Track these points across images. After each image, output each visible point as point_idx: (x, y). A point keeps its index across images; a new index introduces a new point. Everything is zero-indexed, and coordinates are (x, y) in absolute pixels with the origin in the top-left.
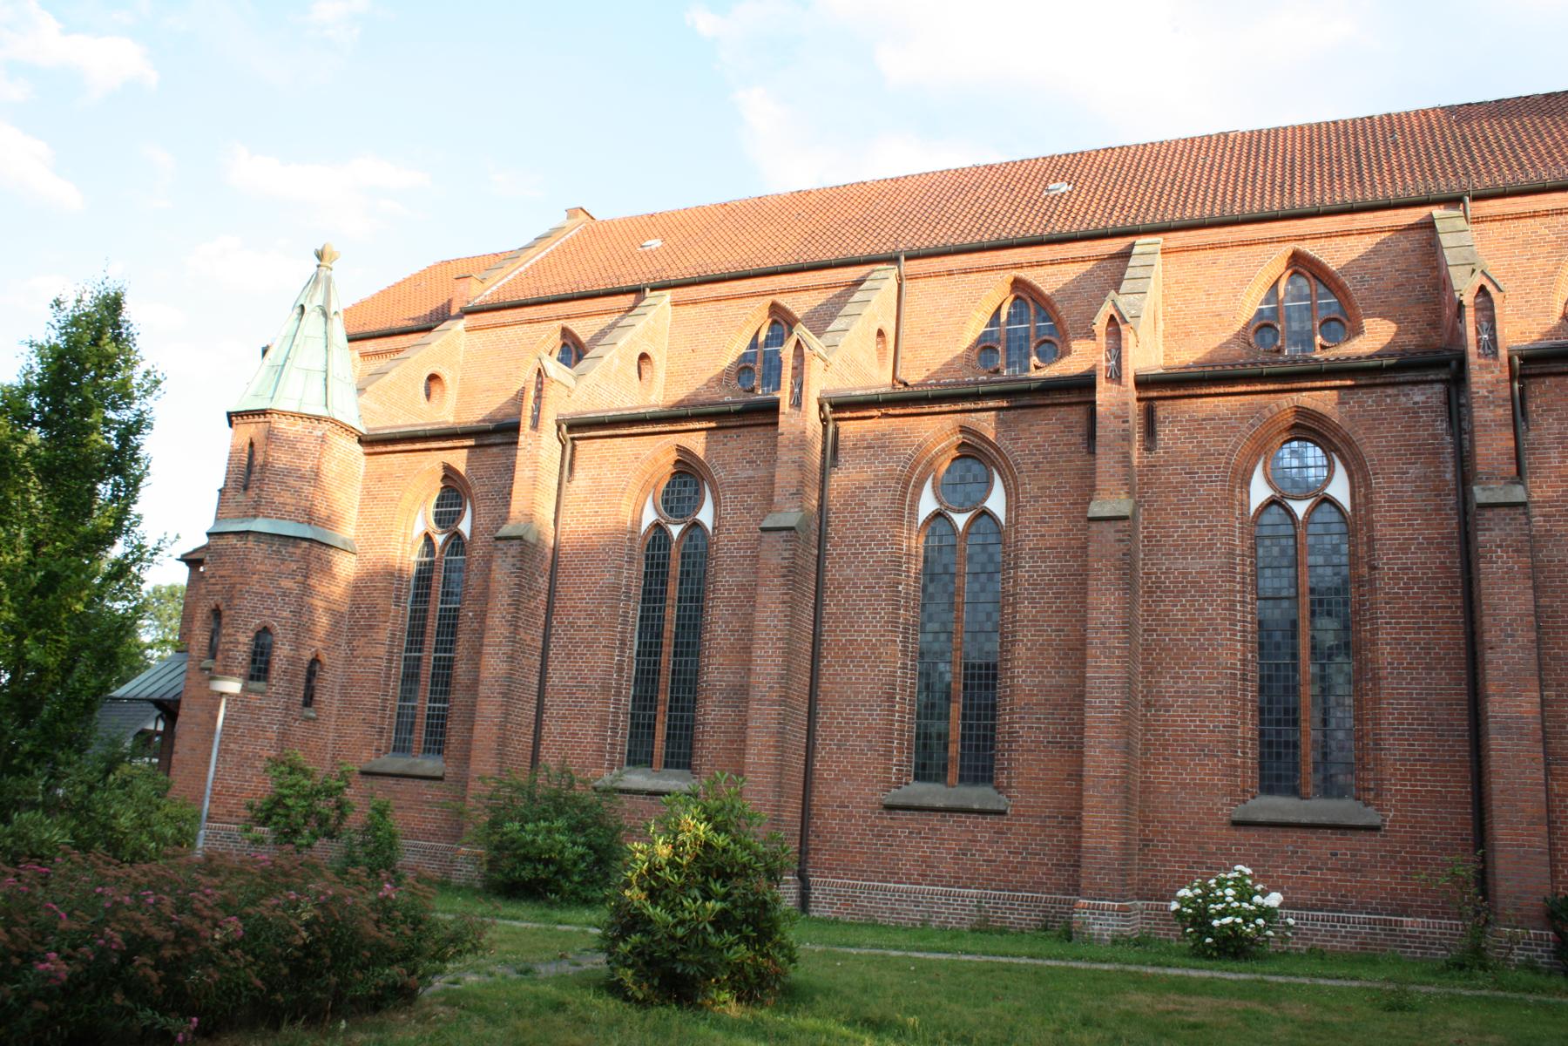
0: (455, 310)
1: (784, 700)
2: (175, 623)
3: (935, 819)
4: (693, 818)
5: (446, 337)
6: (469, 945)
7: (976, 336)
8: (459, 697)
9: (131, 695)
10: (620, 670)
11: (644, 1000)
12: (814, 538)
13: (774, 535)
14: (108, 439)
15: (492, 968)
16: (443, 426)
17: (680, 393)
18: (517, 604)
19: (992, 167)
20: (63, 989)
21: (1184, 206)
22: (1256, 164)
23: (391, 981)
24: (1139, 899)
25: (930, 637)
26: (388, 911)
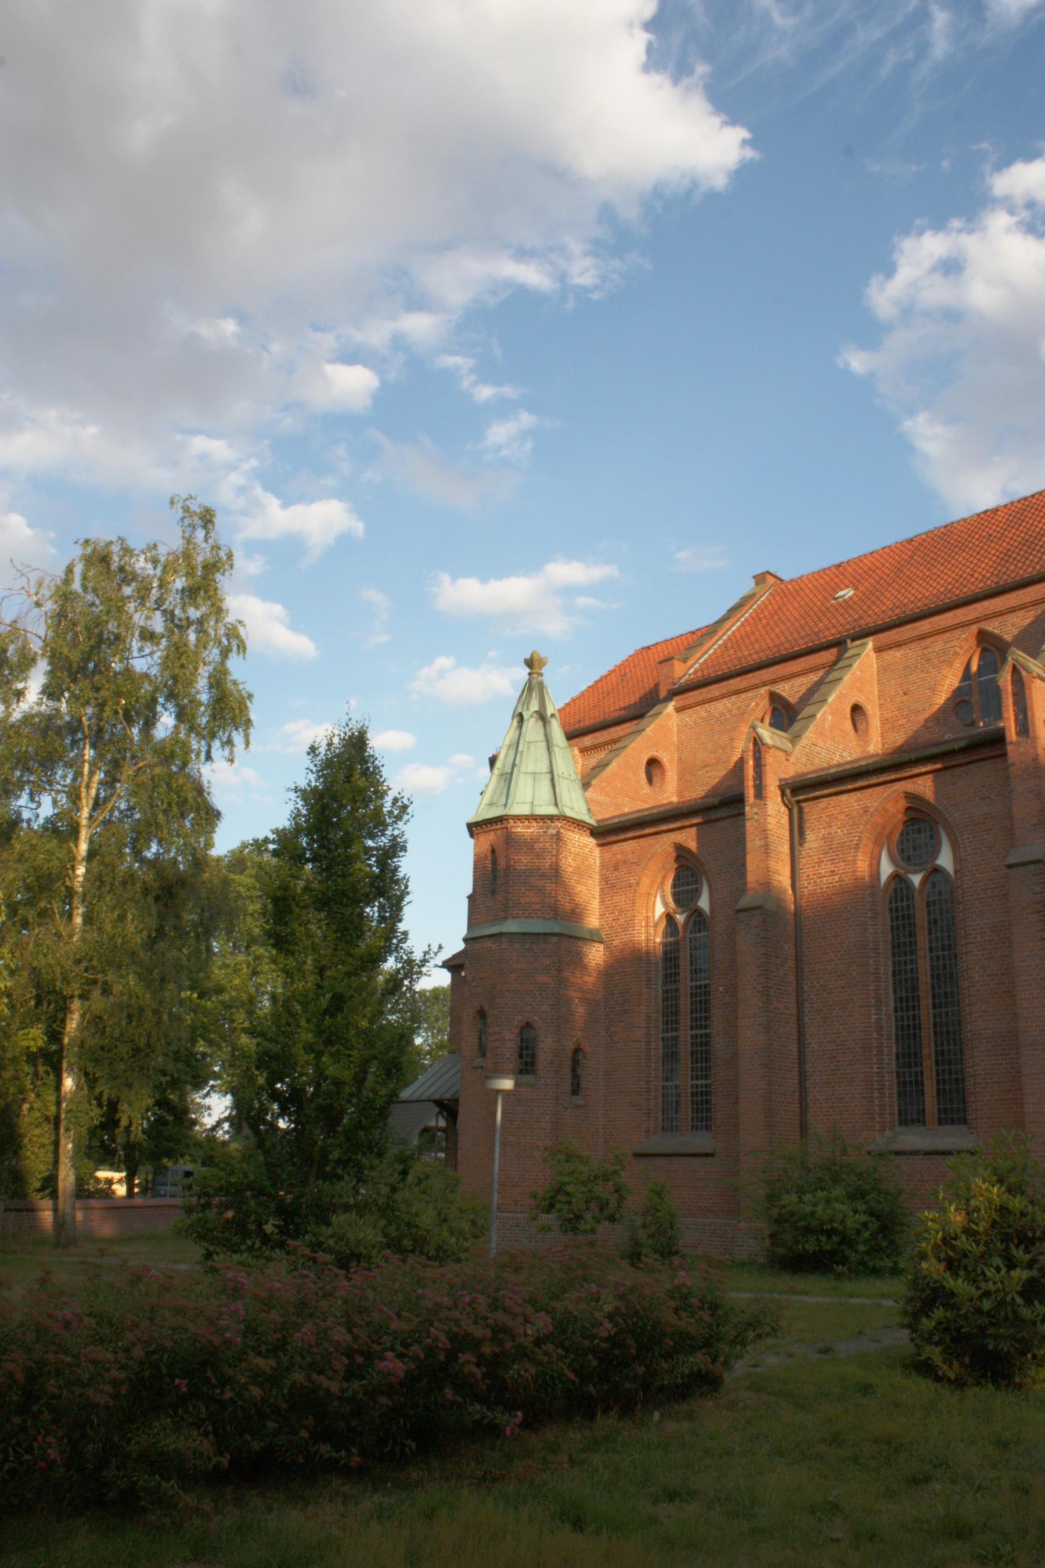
0: (663, 694)
2: (445, 1023)
4: (984, 1181)
5: (658, 721)
6: (767, 1329)
9: (414, 1097)
10: (879, 1028)
14: (370, 866)
16: (668, 807)
17: (898, 738)
20: (402, 1385)
23: (695, 1369)
26: (685, 1297)
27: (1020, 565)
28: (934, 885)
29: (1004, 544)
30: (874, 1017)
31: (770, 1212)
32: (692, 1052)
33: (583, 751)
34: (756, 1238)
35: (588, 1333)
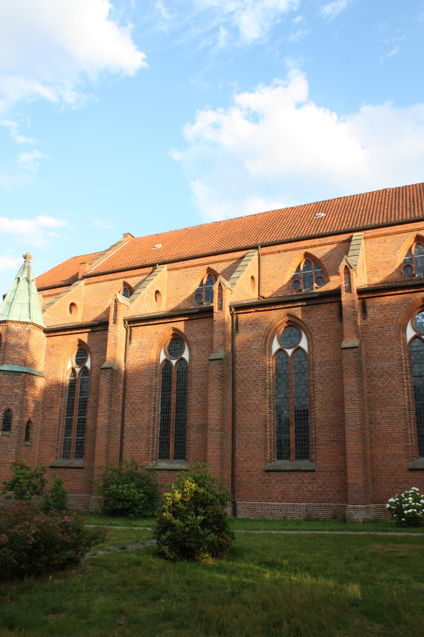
0: (80, 277)
1: (222, 429)
3: (286, 475)
4: (190, 482)
6: (100, 540)
7: (291, 277)
8: (89, 434)
10: (154, 420)
11: (173, 559)
12: (230, 363)
13: (214, 362)
15: (109, 548)
16: (77, 324)
17: (172, 306)
18: (111, 395)
19: (293, 208)
21: (371, 219)
22: (399, 201)
23: (69, 557)
24: (373, 503)
25: (280, 400)
26: (66, 527)
27: (226, 244)
28: (180, 365)
29: (221, 236)
30: (152, 415)
31: (105, 492)
32: (78, 425)
33: (44, 296)
34: (98, 503)
35: (24, 542)
